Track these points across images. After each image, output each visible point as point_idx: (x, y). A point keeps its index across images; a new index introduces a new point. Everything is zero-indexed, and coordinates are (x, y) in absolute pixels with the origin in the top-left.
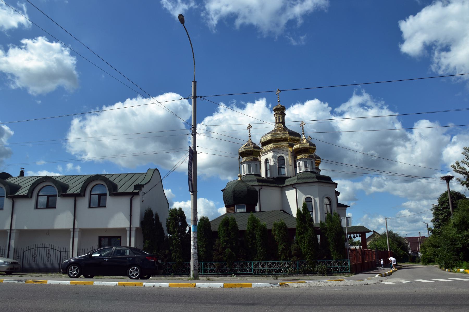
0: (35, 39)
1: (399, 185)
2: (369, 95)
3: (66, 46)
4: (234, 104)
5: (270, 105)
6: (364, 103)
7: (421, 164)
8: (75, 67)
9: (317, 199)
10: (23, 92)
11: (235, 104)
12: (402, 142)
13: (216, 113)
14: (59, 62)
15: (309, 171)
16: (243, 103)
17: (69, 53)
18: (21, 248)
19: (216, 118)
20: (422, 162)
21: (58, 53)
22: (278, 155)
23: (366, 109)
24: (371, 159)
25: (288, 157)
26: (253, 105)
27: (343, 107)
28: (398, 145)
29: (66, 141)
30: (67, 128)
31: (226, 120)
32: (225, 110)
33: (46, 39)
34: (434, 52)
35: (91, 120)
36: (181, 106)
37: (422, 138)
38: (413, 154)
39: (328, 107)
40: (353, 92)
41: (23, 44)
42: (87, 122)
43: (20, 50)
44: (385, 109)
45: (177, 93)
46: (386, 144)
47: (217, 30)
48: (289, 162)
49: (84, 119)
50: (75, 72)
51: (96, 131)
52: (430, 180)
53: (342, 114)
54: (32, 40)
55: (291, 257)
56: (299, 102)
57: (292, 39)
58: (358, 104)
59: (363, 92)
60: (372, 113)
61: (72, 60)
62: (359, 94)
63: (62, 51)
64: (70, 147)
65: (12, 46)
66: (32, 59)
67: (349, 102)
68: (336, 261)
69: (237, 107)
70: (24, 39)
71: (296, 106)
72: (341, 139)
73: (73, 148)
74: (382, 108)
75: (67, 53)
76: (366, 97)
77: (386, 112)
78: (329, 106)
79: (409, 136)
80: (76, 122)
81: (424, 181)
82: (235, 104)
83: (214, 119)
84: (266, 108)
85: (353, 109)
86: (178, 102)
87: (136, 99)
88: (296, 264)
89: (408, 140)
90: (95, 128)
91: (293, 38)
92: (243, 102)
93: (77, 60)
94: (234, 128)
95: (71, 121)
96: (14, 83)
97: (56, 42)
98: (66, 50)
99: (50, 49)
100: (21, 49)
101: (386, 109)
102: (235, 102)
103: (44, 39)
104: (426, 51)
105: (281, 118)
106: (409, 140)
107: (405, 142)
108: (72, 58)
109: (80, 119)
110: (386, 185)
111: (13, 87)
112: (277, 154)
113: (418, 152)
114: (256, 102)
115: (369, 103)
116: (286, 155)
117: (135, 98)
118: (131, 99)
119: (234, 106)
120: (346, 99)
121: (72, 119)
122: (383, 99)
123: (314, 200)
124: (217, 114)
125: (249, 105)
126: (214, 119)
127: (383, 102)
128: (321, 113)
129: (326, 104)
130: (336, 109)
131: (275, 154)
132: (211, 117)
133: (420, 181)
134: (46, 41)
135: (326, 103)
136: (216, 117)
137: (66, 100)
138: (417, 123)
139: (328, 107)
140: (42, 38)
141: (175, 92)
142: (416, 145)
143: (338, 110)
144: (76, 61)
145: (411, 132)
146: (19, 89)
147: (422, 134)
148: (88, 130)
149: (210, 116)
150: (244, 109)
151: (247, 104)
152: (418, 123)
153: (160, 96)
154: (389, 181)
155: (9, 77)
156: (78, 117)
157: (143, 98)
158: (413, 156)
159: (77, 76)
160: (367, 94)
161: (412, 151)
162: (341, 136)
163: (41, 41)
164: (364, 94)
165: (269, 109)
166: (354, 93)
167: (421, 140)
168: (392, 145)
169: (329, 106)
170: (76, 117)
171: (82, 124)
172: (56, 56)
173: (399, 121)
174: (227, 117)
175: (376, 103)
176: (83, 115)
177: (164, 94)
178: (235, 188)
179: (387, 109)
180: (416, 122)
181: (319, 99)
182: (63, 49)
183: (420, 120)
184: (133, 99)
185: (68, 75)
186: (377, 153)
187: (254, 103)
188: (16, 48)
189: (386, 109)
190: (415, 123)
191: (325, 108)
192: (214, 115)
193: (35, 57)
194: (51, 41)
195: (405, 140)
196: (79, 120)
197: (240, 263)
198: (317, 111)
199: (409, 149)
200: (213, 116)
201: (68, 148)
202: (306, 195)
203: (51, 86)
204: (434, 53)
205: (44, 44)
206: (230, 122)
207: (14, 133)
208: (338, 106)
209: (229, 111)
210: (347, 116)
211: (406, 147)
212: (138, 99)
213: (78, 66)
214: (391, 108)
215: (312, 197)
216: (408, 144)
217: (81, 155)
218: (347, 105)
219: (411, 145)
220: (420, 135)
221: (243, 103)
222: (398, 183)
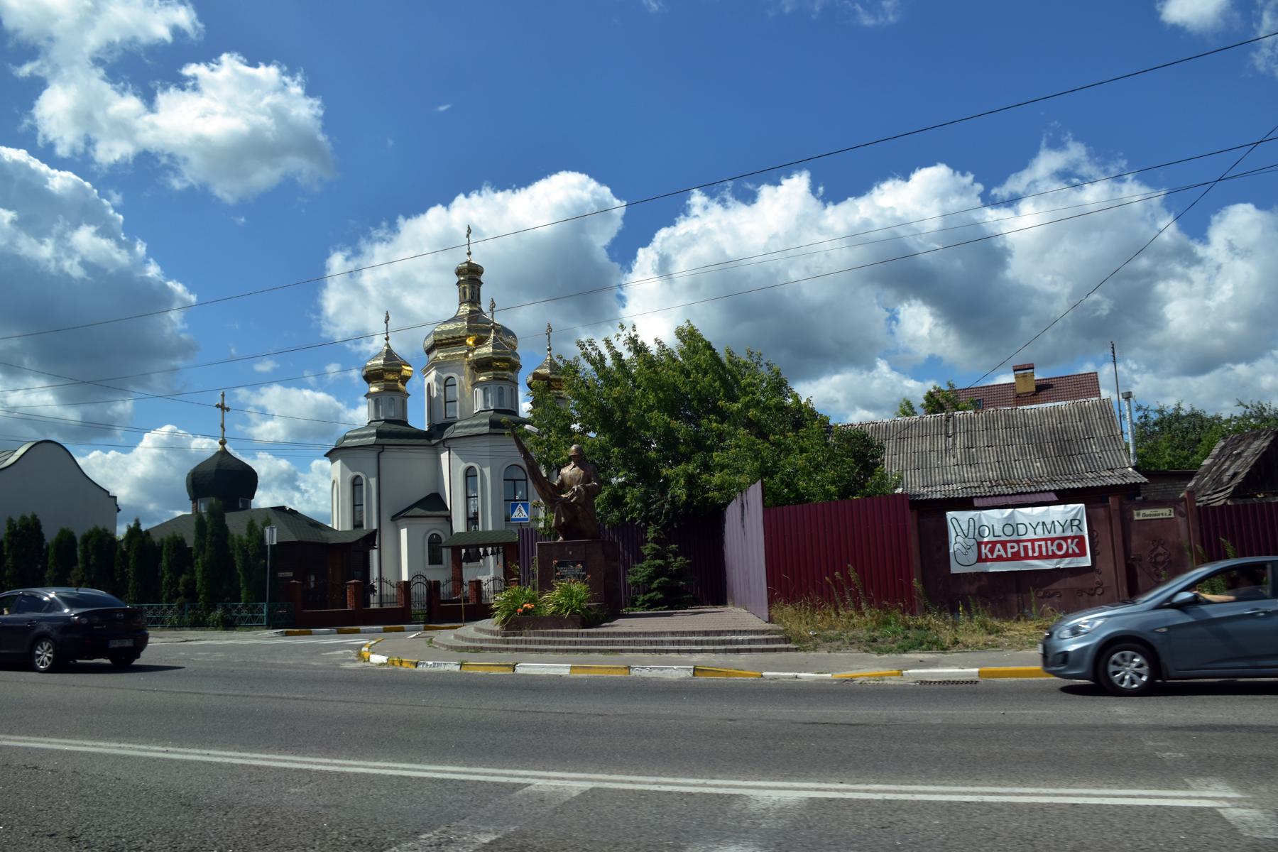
0: (213, 63)
1: (1174, 382)
2: (1086, 146)
3: (291, 73)
4: (727, 189)
5: (821, 189)
6: (1071, 169)
7: (1233, 326)
8: (319, 123)
9: (487, 471)
10: (199, 197)
11: (729, 191)
12: (1179, 269)
13: (682, 217)
14: (279, 114)
15: (492, 410)
16: (749, 186)
17: (302, 89)
18: (993, 526)
19: (683, 232)
20: (1235, 318)
21: (275, 91)
22: (445, 376)
23: (1075, 186)
24: (1093, 315)
25: (463, 378)
26: (777, 191)
27: (1015, 184)
28: (1171, 275)
29: (318, 310)
30: (316, 279)
31: (707, 233)
32: (706, 208)
33: (241, 58)
34: (1261, 15)
35: (373, 256)
36: (592, 205)
37: (1237, 254)
38: (1210, 299)
39: (972, 184)
40: (1042, 140)
41: (187, 79)
42: (363, 262)
43: (181, 92)
44: (1129, 181)
45: (581, 172)
46: (1135, 276)
47: (660, 3)
48: (466, 389)
49: (357, 253)
50: (321, 138)
51: (386, 281)
52: (1260, 364)
53: (1012, 202)
54: (207, 65)
55: (177, 595)
56: (895, 174)
57: (858, 7)
58: (1053, 174)
59: (1068, 140)
60: (1093, 194)
61: (311, 106)
62: (1056, 144)
63: (285, 84)
64: (330, 323)
65: (161, 85)
66: (213, 113)
67: (1031, 168)
68: (245, 606)
69: (737, 199)
70: (187, 65)
71: (888, 186)
72: (1010, 268)
73: (337, 326)
74: (1119, 178)
75: (296, 90)
76: (1076, 151)
77: (1133, 191)
78: (976, 180)
79: (1200, 250)
80: (337, 262)
81: (1242, 369)
82: (729, 191)
83: (677, 234)
84: (810, 195)
85: (1041, 188)
86: (586, 196)
87: (480, 194)
88: (184, 610)
89: (1194, 260)
90: (385, 273)
91: (862, 6)
92: (750, 183)
93: (325, 107)
94: (730, 253)
95: (325, 261)
96: (177, 173)
97: (267, 64)
98: (293, 81)
99: (253, 83)
100: (183, 89)
101: (1133, 180)
102: (730, 186)
103: (237, 60)
104: (1237, 15)
105: (467, 290)
106: (1199, 261)
107: (1188, 267)
108: (311, 101)
109: (346, 254)
110: (1137, 383)
111: (177, 184)
112: (443, 374)
113: (1225, 291)
114: (785, 182)
115: (1085, 169)
116: (460, 374)
117: (477, 192)
118: (467, 196)
119: (728, 197)
120: (1022, 162)
121: (328, 256)
122: (1121, 154)
123: (482, 472)
124: (685, 220)
125: (766, 191)
126: (677, 234)
127: (1124, 163)
128: (955, 203)
129: (967, 176)
130: (994, 191)
131: (439, 374)
132: (671, 230)
133: (1230, 369)
134: (241, 62)
135: (968, 173)
136: (684, 227)
137: (303, 211)
138: (1220, 213)
139: (972, 184)
140: (232, 56)
141: (574, 170)
142: (1218, 273)
143: (1002, 192)
144: (322, 108)
145: (1204, 239)
146: (191, 189)
147: (1234, 243)
148: (367, 278)
149: (668, 226)
150: (754, 202)
151: (760, 189)
152: (1221, 216)
153: (536, 183)
154: (1145, 373)
155: (164, 160)
156: (341, 250)
157: (495, 192)
158: (1211, 304)
159: (328, 147)
160: (1079, 144)
161: (1208, 292)
162: (1009, 259)
163: (230, 64)
164: (1071, 145)
165: (818, 199)
166: (1043, 144)
167: (1233, 259)
168: (1152, 276)
169: (976, 180)
170: (335, 250)
171: (351, 266)
172: (268, 99)
173: (1169, 211)
174: (711, 226)
175: (1102, 168)
176: (353, 242)
177: (547, 178)
178: (219, 465)
179: (1135, 181)
180: (1216, 212)
181: (950, 165)
182: (287, 79)
183: (1226, 207)
184: (471, 194)
185: (302, 143)
186: (1108, 300)
187: (778, 183)
188: (172, 90)
189: (1133, 180)
190: (1212, 217)
191: (965, 187)
192: (677, 224)
193: (220, 108)
194: (253, 63)
195: (1187, 263)
196: (344, 255)
197: (162, 607)
198: (944, 197)
199: (1199, 285)
200: (675, 225)
201: (325, 327)
202: (353, 471)
203: (264, 177)
204: (1259, 20)
205: (236, 72)
206: (719, 238)
207: (197, 298)
208: (1001, 181)
209: (716, 209)
210: (1026, 207)
211: (1190, 282)
212: (483, 192)
213: (328, 122)
214: (1145, 175)
215: (363, 476)
216: (1197, 274)
217: (358, 344)
218: (1026, 176)
219: (1204, 276)
220: (1231, 247)
221: (749, 186)
222: (1169, 376)
